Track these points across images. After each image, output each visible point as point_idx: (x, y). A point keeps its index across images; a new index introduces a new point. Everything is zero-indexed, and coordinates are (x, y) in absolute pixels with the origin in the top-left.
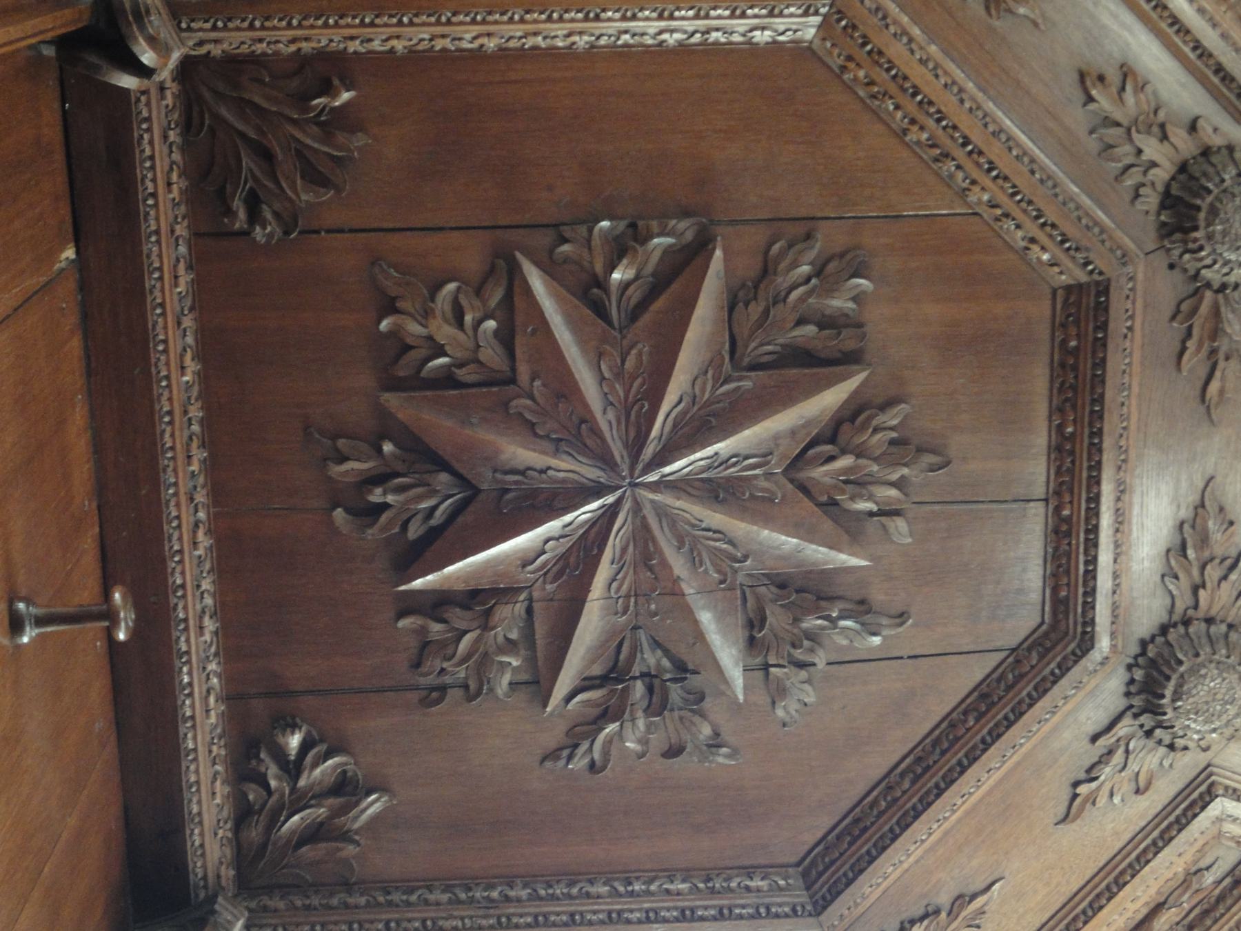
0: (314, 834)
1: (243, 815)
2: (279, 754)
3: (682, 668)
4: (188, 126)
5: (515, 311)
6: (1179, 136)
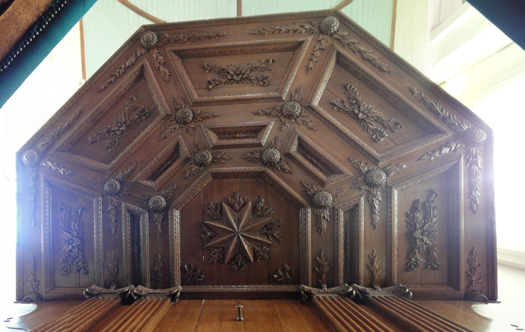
0: (290, 274)
1: (287, 283)
2: (277, 278)
3: (266, 226)
4: (190, 285)
5: (213, 247)
6: (192, 166)
